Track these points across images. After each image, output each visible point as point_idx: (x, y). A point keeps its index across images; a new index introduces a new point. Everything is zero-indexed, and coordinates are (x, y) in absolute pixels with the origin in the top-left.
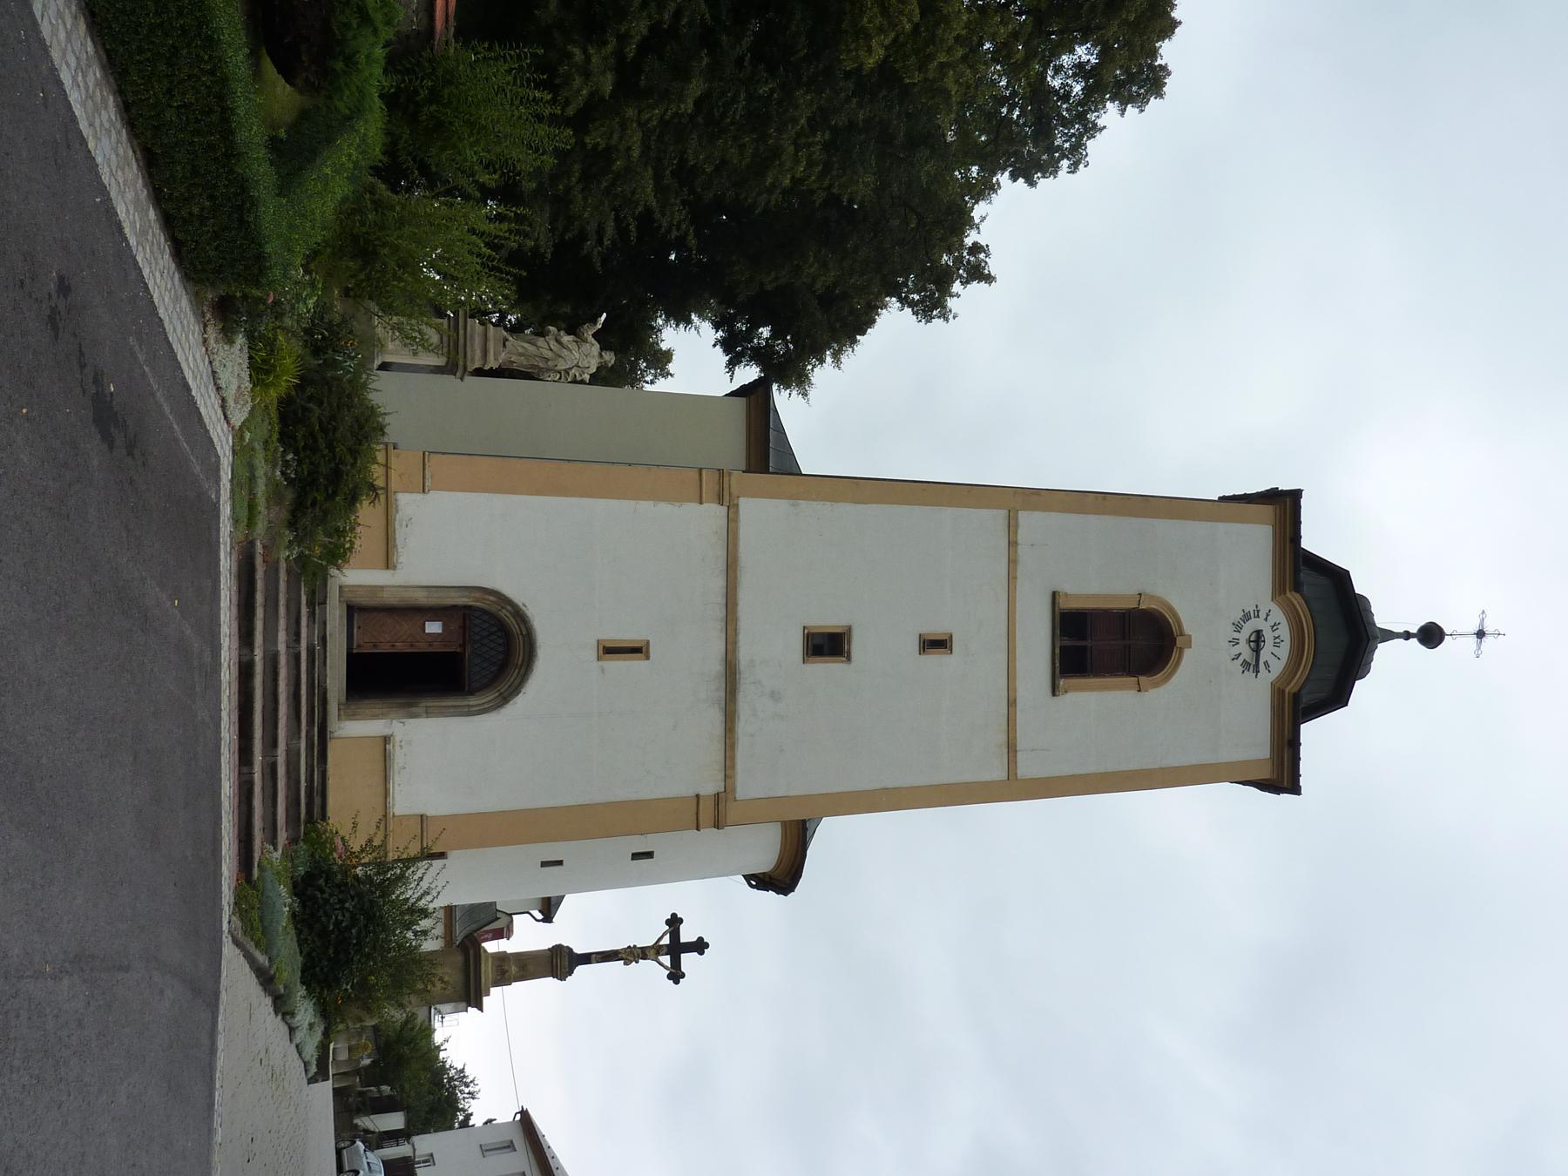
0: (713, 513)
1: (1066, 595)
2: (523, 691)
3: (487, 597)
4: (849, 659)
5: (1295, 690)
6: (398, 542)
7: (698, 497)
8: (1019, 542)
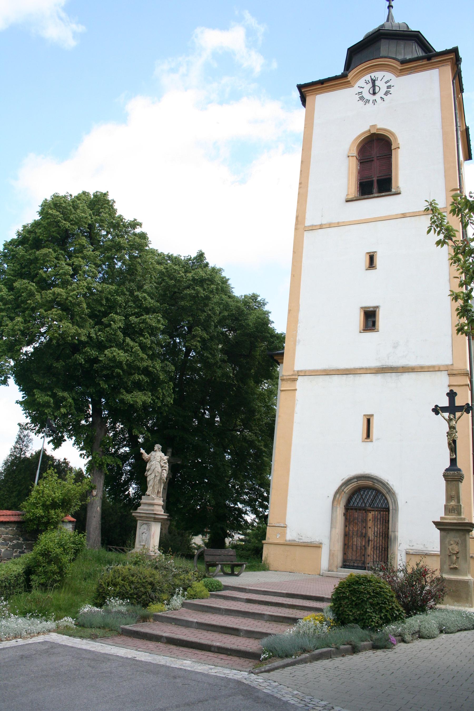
0: (301, 383)
1: (347, 195)
2: (386, 481)
3: (337, 499)
4: (377, 307)
5: (399, 63)
6: (309, 541)
7: (293, 392)
8: (320, 223)
